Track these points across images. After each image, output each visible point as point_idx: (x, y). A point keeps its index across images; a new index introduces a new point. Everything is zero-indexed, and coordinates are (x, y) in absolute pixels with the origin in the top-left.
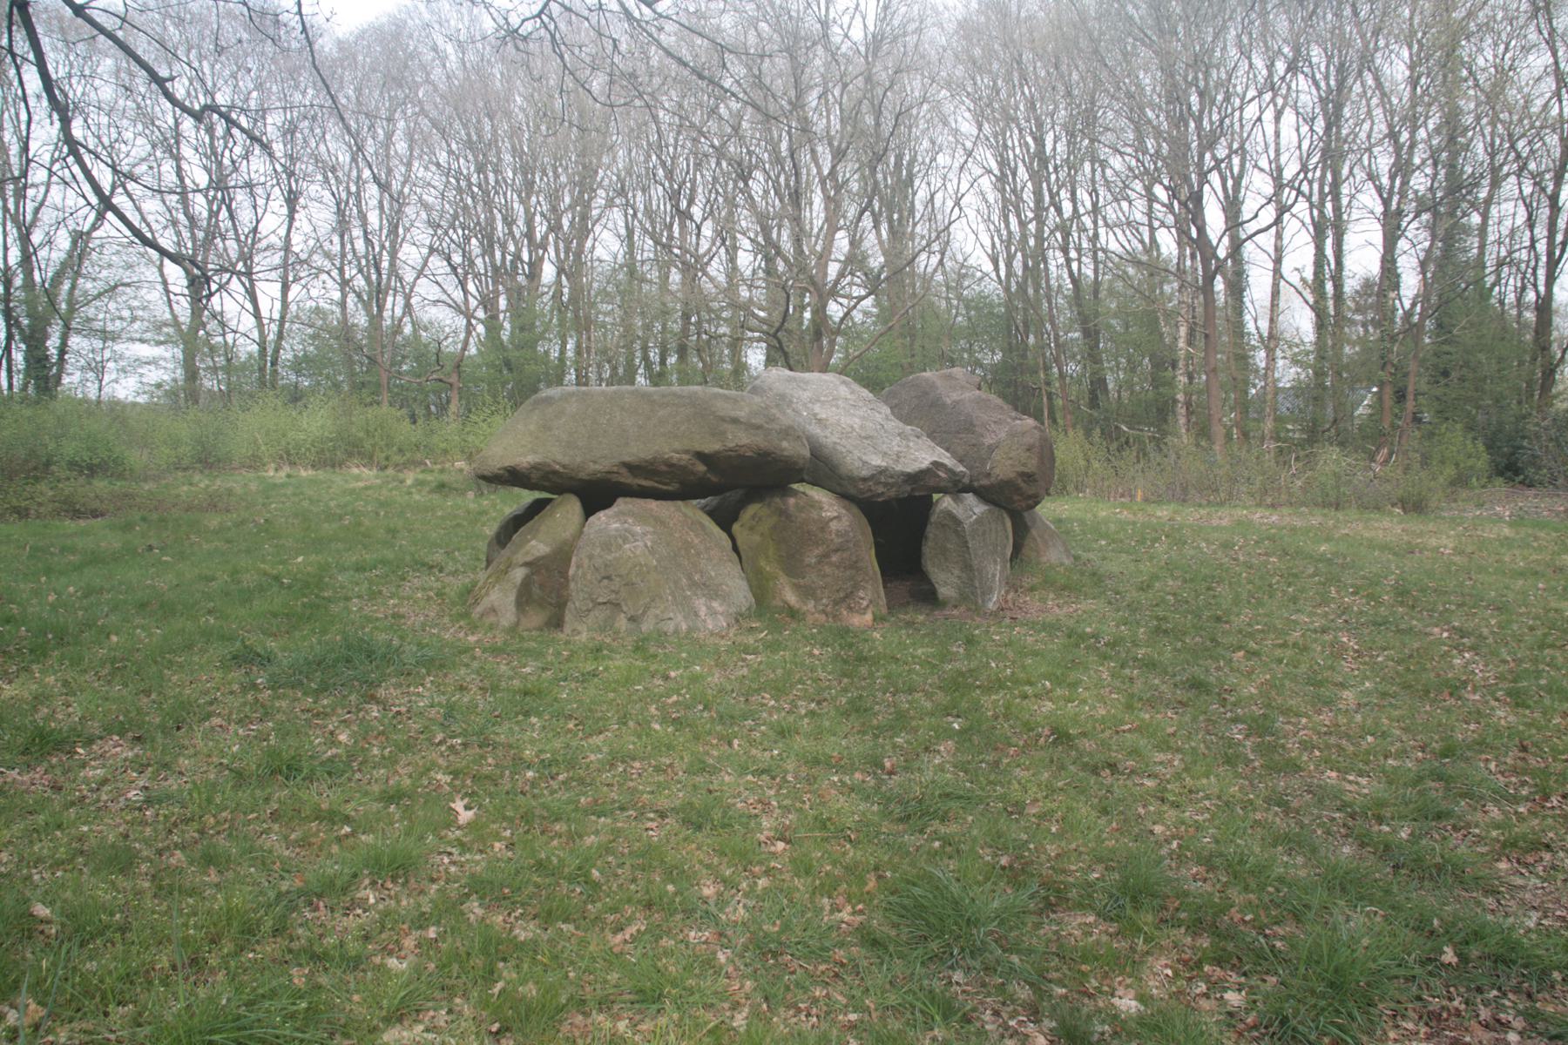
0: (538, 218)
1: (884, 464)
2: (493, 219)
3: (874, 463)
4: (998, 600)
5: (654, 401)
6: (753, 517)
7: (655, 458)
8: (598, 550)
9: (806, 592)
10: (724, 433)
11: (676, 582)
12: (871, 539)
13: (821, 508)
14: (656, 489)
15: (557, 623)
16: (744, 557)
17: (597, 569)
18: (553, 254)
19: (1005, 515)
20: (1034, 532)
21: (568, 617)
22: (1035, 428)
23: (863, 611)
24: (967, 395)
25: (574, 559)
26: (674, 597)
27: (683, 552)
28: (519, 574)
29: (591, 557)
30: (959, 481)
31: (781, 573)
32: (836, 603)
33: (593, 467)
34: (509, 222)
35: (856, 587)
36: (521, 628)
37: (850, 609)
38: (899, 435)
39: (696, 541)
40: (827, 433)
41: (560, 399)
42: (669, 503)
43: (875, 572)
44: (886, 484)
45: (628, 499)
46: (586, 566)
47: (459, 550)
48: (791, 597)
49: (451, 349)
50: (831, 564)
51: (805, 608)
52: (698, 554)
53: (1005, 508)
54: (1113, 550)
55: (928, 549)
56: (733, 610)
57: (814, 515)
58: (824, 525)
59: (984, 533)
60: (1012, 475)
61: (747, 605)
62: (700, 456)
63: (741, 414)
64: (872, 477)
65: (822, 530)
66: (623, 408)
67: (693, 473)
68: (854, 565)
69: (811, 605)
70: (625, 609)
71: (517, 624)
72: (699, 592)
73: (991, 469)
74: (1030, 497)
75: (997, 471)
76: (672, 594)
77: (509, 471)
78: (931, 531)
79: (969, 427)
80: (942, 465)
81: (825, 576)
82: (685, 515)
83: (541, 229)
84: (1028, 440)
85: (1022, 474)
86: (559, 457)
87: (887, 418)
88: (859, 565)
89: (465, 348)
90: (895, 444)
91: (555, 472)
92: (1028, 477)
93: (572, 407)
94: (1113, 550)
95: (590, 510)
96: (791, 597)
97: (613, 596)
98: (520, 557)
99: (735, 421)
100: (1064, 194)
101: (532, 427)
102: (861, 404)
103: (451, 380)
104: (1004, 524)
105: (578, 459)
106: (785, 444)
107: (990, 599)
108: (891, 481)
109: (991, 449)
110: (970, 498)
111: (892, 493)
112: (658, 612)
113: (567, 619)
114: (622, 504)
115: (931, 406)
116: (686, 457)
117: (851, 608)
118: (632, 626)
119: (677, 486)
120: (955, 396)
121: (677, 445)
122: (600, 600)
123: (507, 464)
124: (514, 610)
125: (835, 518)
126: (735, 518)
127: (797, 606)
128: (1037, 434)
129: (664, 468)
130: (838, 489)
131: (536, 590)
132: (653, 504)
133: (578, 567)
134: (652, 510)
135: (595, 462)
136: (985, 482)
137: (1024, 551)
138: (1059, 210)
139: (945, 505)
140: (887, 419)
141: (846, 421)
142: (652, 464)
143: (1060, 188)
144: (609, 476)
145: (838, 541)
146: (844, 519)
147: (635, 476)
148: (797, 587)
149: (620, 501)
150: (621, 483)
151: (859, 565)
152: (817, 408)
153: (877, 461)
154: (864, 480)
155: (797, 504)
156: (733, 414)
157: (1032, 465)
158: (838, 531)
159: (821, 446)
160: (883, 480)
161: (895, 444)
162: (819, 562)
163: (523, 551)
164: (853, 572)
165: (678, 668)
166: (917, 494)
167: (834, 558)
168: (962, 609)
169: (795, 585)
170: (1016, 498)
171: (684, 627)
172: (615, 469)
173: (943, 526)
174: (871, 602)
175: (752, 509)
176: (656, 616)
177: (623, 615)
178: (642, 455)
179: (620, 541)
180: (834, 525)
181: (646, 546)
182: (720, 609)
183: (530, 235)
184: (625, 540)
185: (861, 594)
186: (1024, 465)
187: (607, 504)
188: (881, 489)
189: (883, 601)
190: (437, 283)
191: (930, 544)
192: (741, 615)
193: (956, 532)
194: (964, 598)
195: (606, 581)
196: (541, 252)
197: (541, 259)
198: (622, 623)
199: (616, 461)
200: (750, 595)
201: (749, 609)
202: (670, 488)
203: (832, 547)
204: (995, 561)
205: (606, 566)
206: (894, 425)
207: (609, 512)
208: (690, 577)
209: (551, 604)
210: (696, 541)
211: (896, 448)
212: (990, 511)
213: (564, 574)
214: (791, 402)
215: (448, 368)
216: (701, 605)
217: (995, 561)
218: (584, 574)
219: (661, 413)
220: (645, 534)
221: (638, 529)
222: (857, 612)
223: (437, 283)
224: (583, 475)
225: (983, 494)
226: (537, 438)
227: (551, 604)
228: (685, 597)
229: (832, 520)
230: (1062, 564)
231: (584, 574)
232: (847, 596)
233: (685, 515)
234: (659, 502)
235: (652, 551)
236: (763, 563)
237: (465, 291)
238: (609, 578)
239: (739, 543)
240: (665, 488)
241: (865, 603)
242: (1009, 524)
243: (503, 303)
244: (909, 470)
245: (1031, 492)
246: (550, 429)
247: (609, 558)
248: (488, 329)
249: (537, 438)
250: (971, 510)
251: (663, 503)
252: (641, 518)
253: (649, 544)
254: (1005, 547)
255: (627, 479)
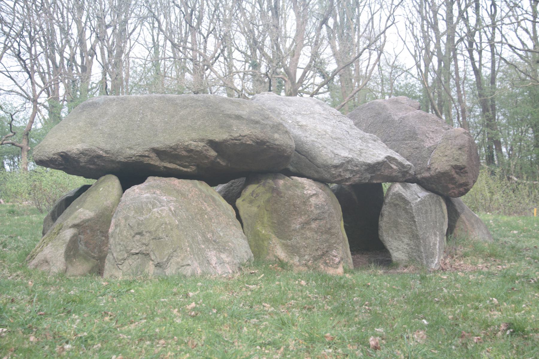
0: (88, 33)
1: (350, 156)
2: (53, 31)
3: (342, 155)
4: (438, 263)
5: (177, 104)
6: (252, 194)
7: (177, 145)
8: (133, 213)
9: (293, 250)
10: (230, 127)
11: (193, 238)
12: (341, 213)
13: (304, 188)
14: (175, 169)
15: (99, 271)
16: (245, 224)
17: (131, 227)
18: (100, 59)
19: (442, 201)
20: (463, 216)
21: (108, 265)
22: (465, 133)
23: (337, 266)
24: (411, 113)
25: (113, 221)
26: (191, 248)
27: (199, 216)
28: (68, 234)
29: (126, 218)
30: (407, 172)
31: (273, 236)
32: (315, 259)
33: (129, 152)
34: (65, 32)
35: (330, 247)
36: (68, 274)
37: (326, 264)
38: (360, 139)
39: (209, 209)
40: (307, 134)
41: (103, 104)
42: (189, 181)
43: (344, 238)
44: (352, 172)
45: (157, 178)
46: (122, 224)
47: (21, 235)
48: (281, 254)
49: (22, 124)
50: (311, 229)
51: (291, 262)
52: (210, 219)
53: (441, 195)
54: (524, 236)
55: (384, 223)
56: (237, 261)
57: (298, 192)
58: (305, 200)
59: (426, 212)
60: (447, 168)
61: (247, 258)
62: (212, 144)
63: (244, 113)
64: (342, 165)
65: (304, 203)
66: (152, 110)
67: (206, 157)
68: (328, 231)
69: (296, 260)
70: (153, 257)
71: (66, 271)
72: (211, 246)
73: (431, 164)
74: (461, 185)
75: (435, 166)
76: (190, 246)
77: (62, 156)
78: (386, 210)
79: (413, 135)
80: (394, 159)
81: (306, 239)
82: (200, 190)
83: (90, 40)
84: (459, 141)
85: (455, 167)
86: (103, 145)
87: (351, 128)
88: (333, 231)
89: (32, 122)
90: (358, 145)
91: (99, 157)
92: (460, 169)
93: (113, 109)
94: (524, 236)
95: (125, 186)
96: (281, 254)
97: (144, 247)
98: (71, 221)
99: (239, 117)
100: (470, 10)
101: (81, 124)
102: (331, 117)
103: (21, 145)
104: (441, 207)
105: (118, 146)
106: (276, 136)
107: (432, 262)
108: (355, 168)
109: (431, 150)
110: (415, 187)
111: (356, 179)
112: (179, 260)
113: (106, 267)
114: (151, 181)
115: (383, 122)
116: (201, 144)
117: (327, 264)
118: (159, 271)
119: (194, 168)
120: (401, 115)
121: (194, 135)
122: (134, 251)
123: (60, 150)
124: (63, 260)
125: (314, 195)
126: (239, 195)
127: (286, 260)
128: (466, 137)
129: (184, 153)
130: (316, 176)
131: (82, 247)
132: (175, 181)
133: (116, 226)
134: (175, 185)
135: (131, 148)
136: (426, 174)
137: (455, 231)
138: (466, 20)
139: (396, 189)
140: (351, 128)
141: (320, 127)
142: (175, 150)
143: (467, 6)
144: (141, 159)
145: (316, 212)
146: (321, 196)
147: (162, 160)
148: (286, 247)
149: (150, 179)
150: (150, 164)
151: (333, 231)
152: (299, 118)
153: (345, 154)
154: (336, 167)
155: (285, 185)
156: (237, 113)
157: (463, 160)
158: (316, 205)
159: (302, 143)
160: (350, 168)
161: (358, 145)
162: (303, 228)
163: (73, 216)
164: (328, 236)
165: (195, 291)
166: (375, 182)
167: (314, 225)
168: (411, 268)
169: (284, 244)
170: (451, 186)
171: (199, 271)
172: (147, 154)
173: (395, 205)
174: (342, 259)
175: (251, 188)
176: (178, 263)
177: (151, 262)
178: (168, 143)
179: (150, 206)
180: (313, 200)
181: (170, 210)
182: (227, 260)
183: (81, 42)
184: (154, 206)
185: (334, 253)
186: (457, 160)
187: (140, 180)
188: (348, 175)
189: (351, 260)
190: (10, 77)
191: (385, 219)
192: (243, 265)
193: (405, 209)
194: (412, 260)
195: (138, 237)
196: (90, 58)
197: (91, 62)
198: (150, 268)
199: (147, 147)
200: (250, 251)
201: (249, 260)
202: (189, 170)
203: (311, 216)
204: (435, 234)
205: (139, 224)
206: (357, 132)
207: (142, 186)
208: (204, 235)
209: (94, 258)
210: (209, 209)
211: (359, 147)
212: (430, 196)
213: (105, 234)
214: (279, 114)
215: (19, 135)
216: (213, 256)
217: (435, 234)
218: (121, 231)
219: (182, 113)
220: (169, 202)
221: (164, 198)
222: (331, 266)
223: (10, 77)
224: (121, 158)
225: (424, 184)
226: (85, 132)
227: (94, 258)
228: (200, 249)
229: (311, 196)
230: (486, 242)
231: (121, 231)
232: (323, 255)
233: (200, 190)
234: (180, 180)
235: (175, 214)
236: (259, 228)
237: (33, 83)
238: (140, 234)
239: (241, 213)
240: (185, 169)
241: (337, 260)
242: (445, 207)
243: (62, 91)
244: (369, 162)
245: (462, 181)
246: (95, 125)
247: (142, 218)
248: (51, 113)
249: (85, 132)
250: (416, 194)
251: (183, 180)
252: (166, 191)
253: (173, 209)
254: (442, 224)
255: (155, 161)
